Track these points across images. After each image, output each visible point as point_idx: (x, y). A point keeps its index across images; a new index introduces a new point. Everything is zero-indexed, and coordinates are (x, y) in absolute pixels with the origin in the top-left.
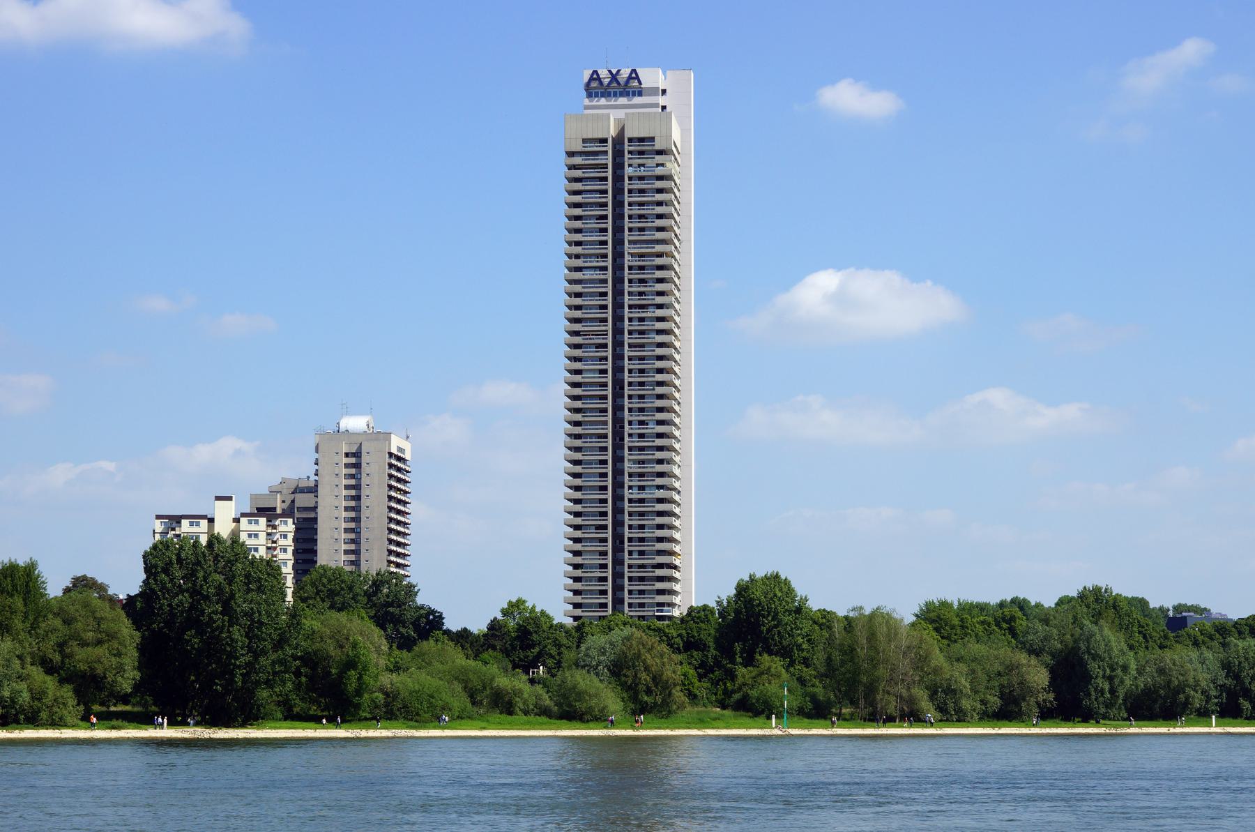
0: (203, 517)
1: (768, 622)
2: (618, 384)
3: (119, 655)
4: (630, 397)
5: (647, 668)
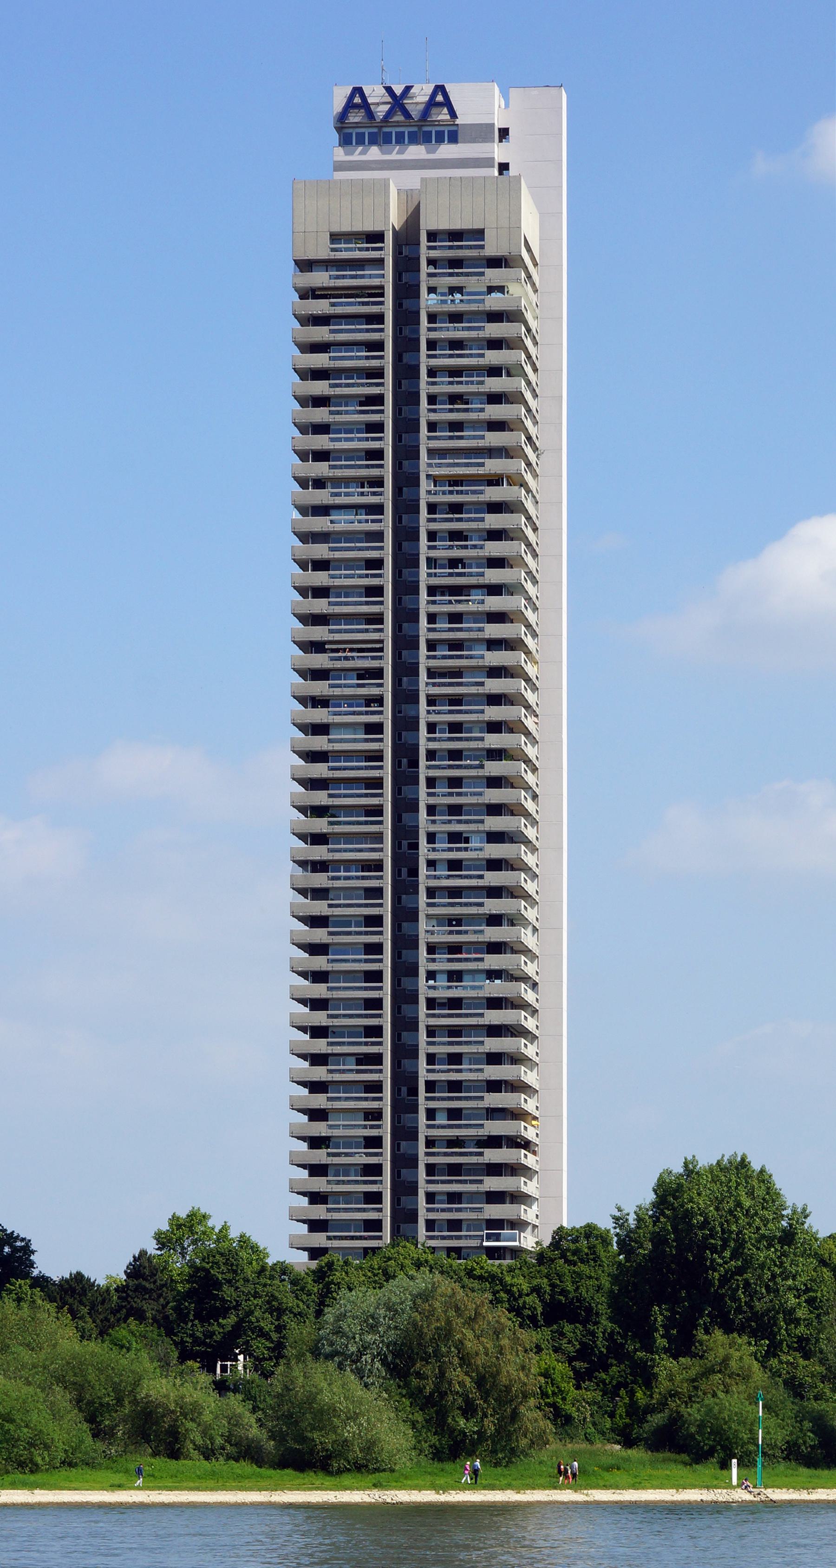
1: (722, 1262)
2: (406, 755)
4: (431, 1032)
5: (465, 1360)
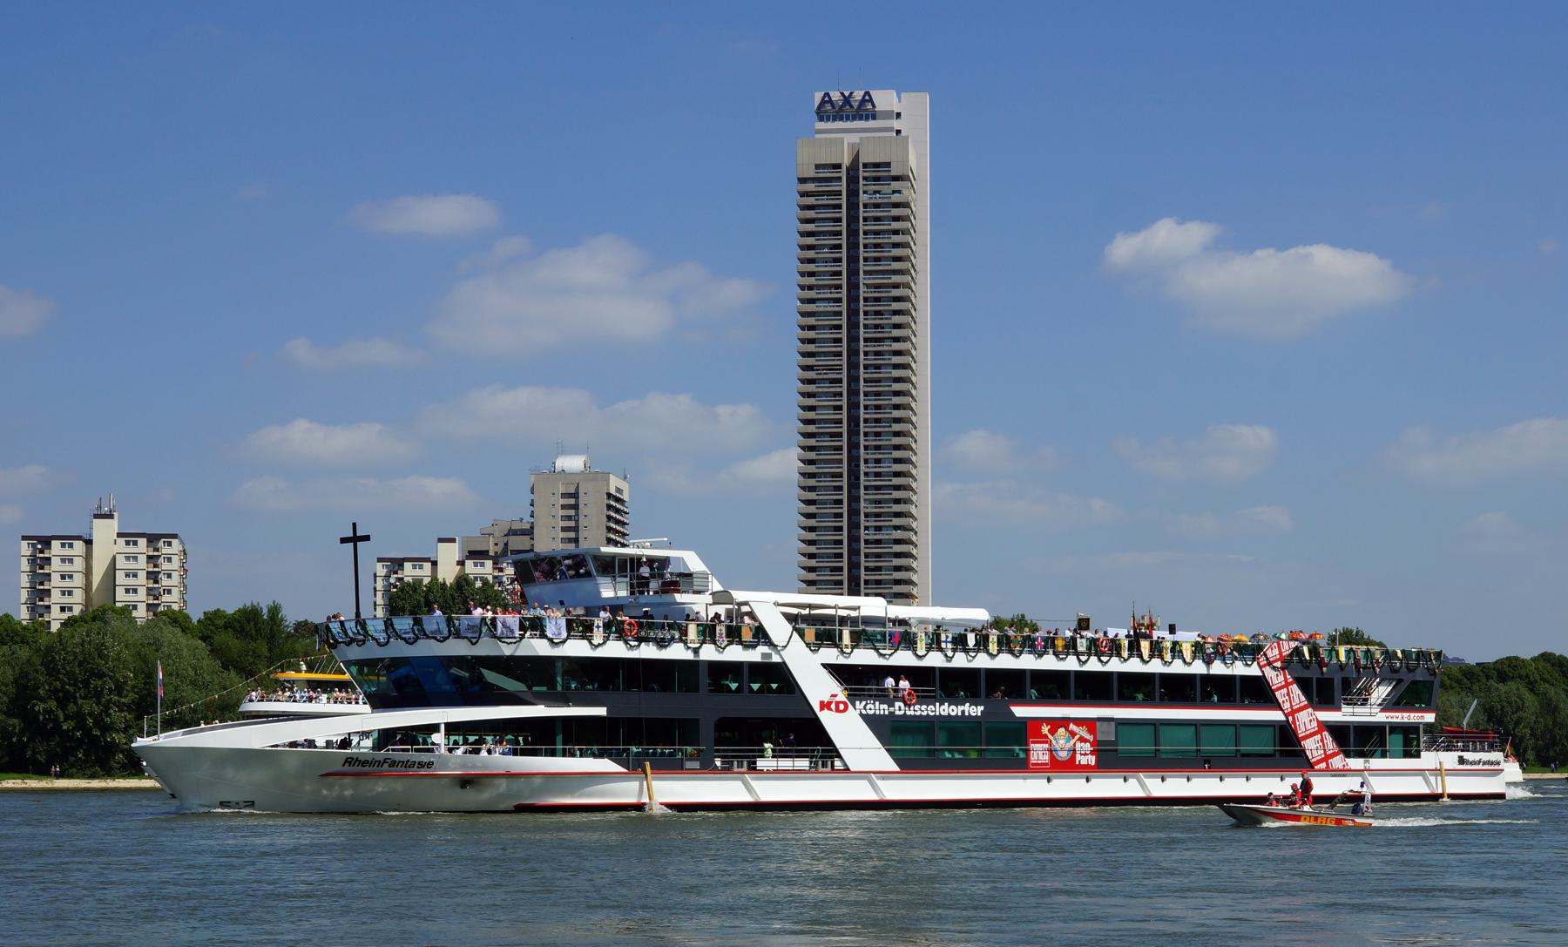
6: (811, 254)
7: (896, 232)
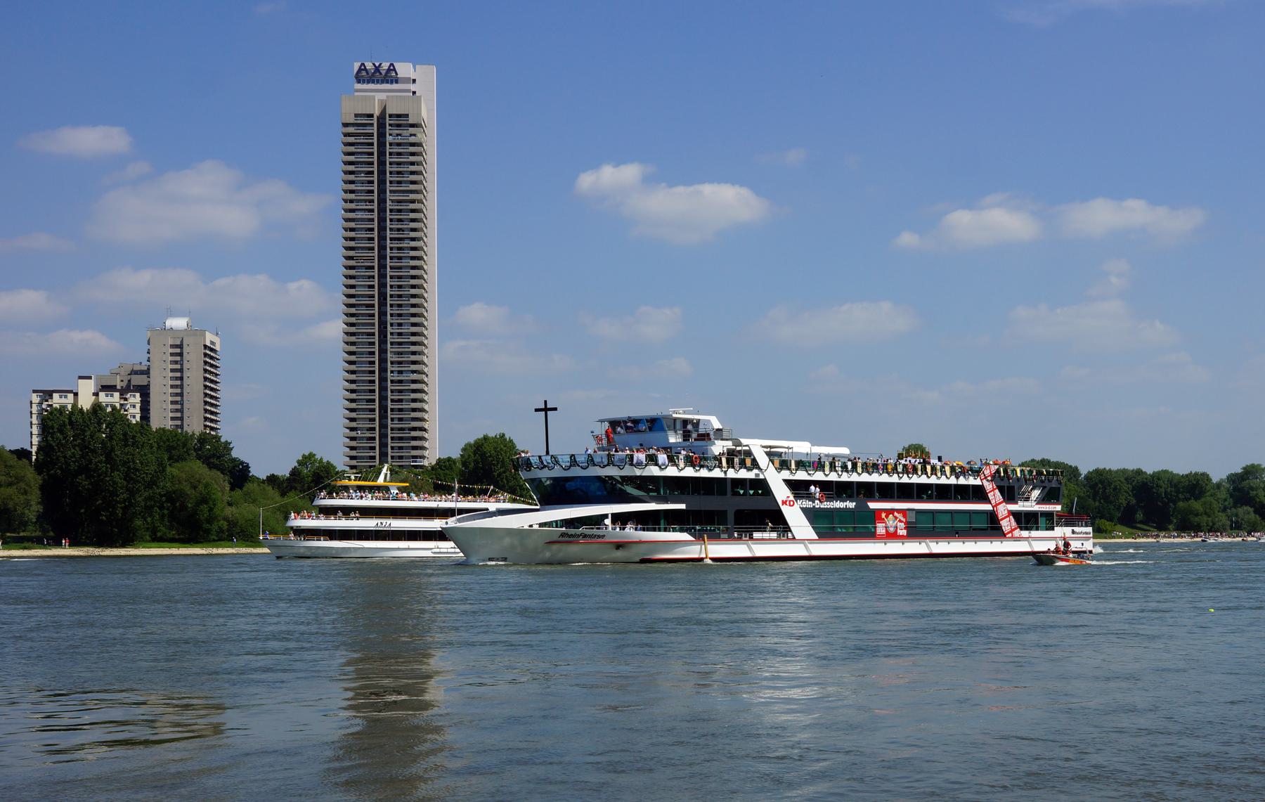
0: (70, 392)
3: (26, 493)
4: (391, 306)
6: (352, 177)
7: (413, 164)
